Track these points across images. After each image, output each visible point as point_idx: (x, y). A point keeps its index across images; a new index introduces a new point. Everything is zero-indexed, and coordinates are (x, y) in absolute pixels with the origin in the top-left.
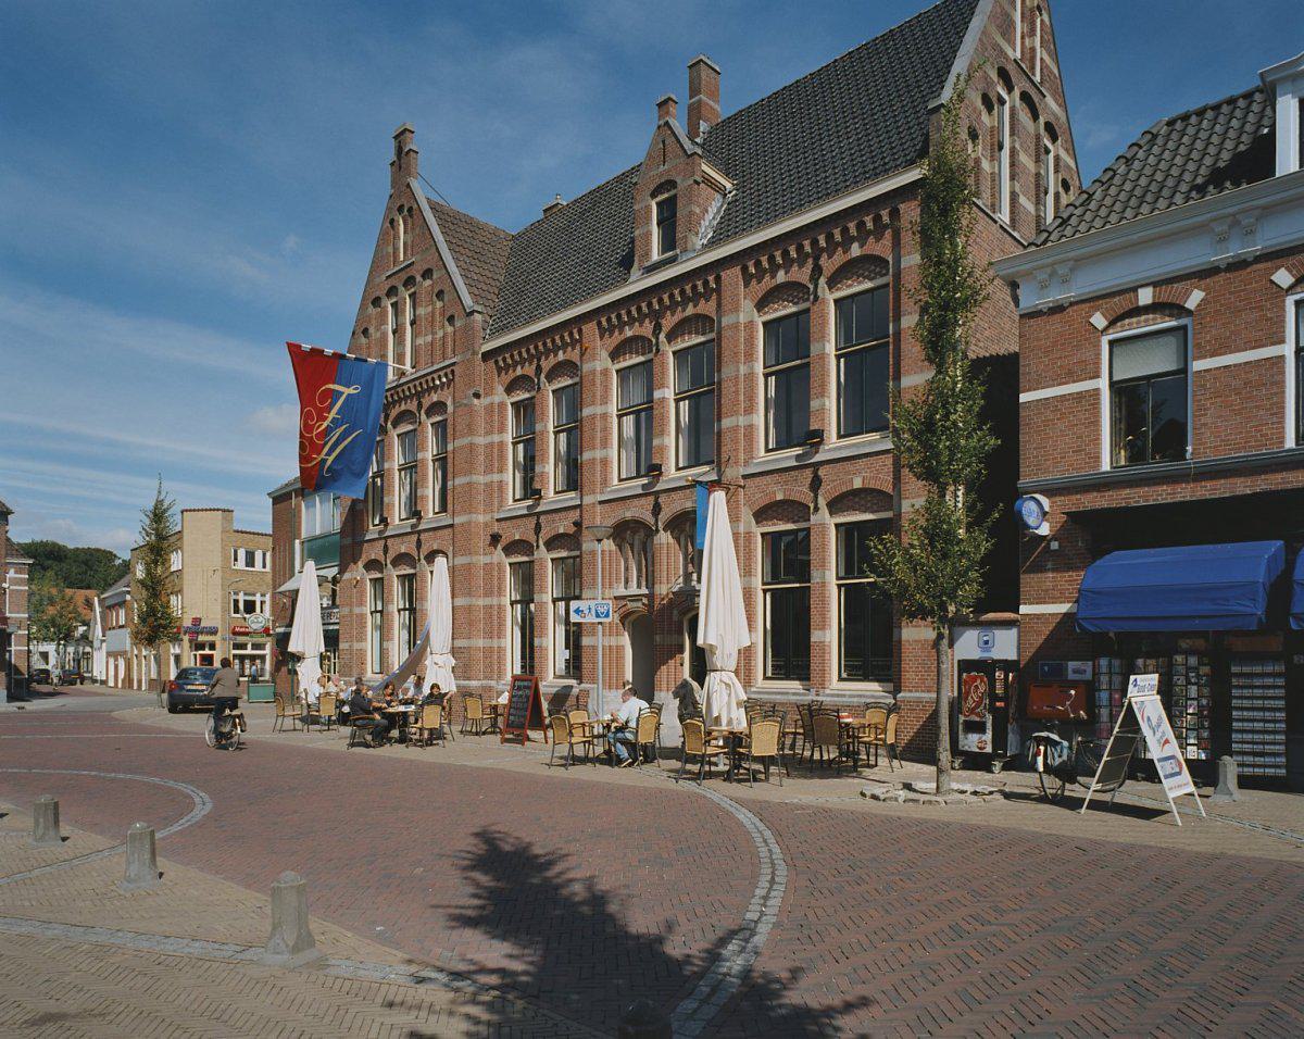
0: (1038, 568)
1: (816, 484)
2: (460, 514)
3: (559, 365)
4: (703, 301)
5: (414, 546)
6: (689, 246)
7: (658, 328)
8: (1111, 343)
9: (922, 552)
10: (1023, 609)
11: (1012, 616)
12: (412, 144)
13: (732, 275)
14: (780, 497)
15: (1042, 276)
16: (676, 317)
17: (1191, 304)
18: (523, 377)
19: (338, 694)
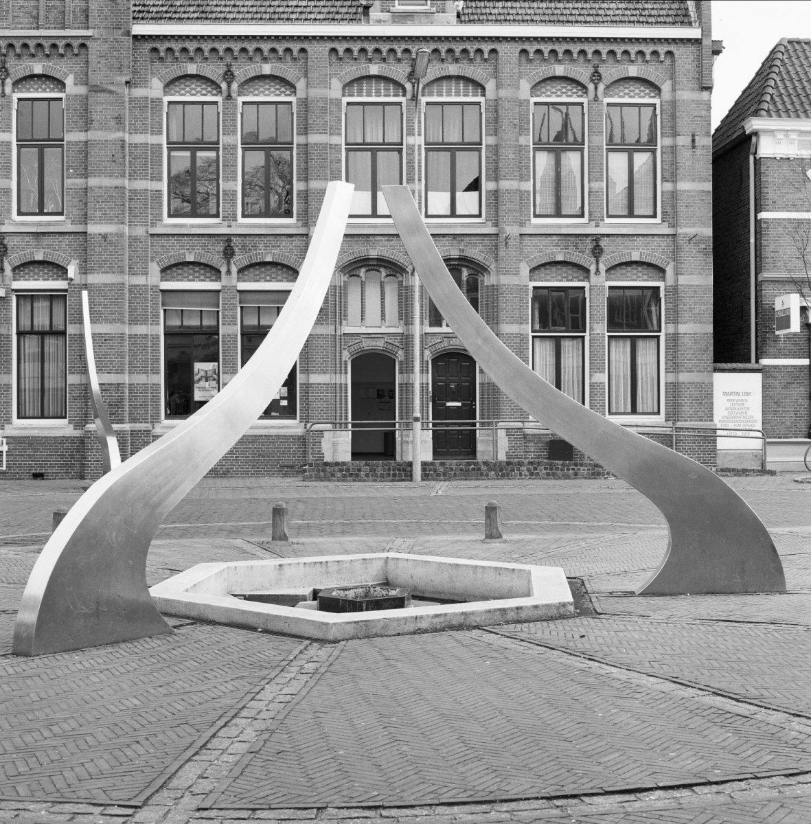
7: (596, 77)
13: (508, 53)
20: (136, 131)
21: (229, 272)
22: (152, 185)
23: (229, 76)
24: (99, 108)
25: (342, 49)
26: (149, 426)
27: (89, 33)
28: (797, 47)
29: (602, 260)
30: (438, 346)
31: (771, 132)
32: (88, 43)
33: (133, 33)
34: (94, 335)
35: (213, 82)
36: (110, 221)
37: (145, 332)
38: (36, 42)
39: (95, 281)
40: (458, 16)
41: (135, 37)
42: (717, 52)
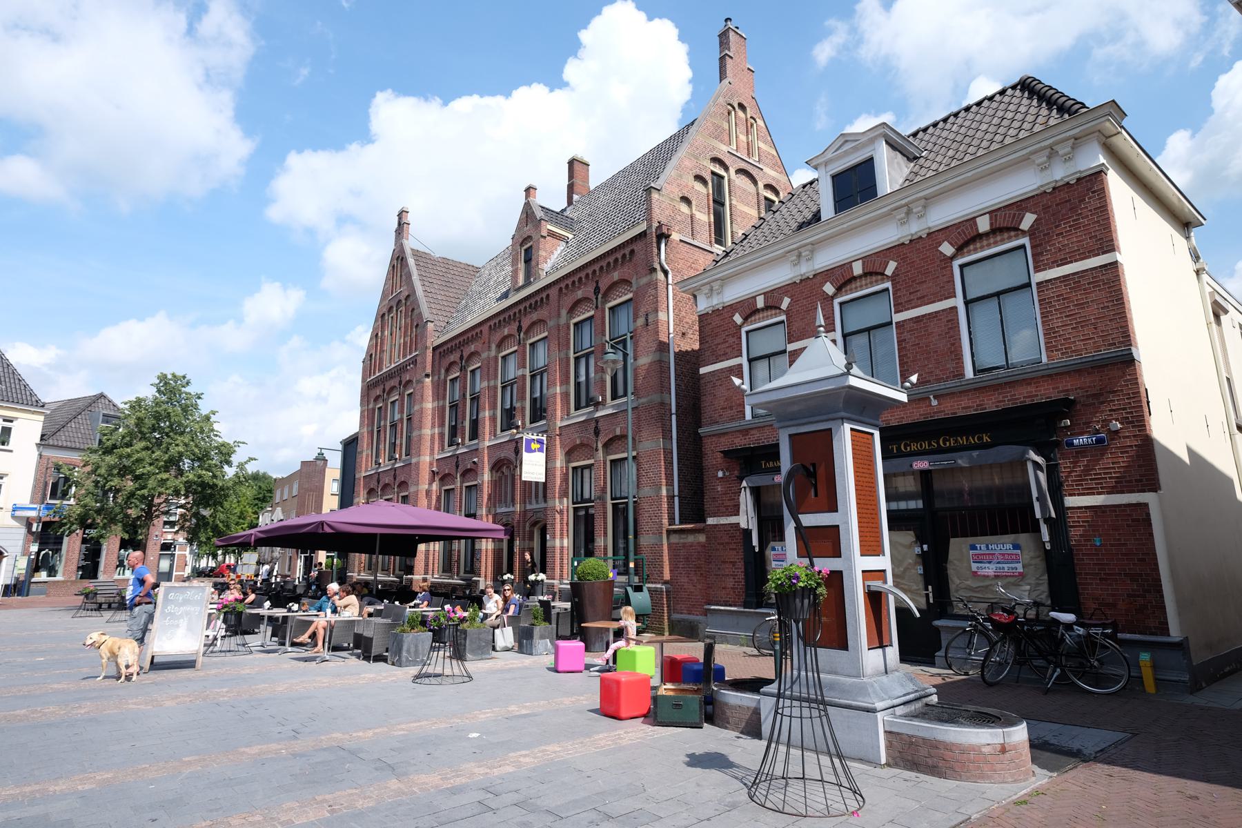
1: (597, 432)
3: (533, 324)
5: (392, 479)
8: (841, 304)
10: (711, 521)
12: (410, 218)
15: (901, 214)
18: (510, 336)
19: (1025, 613)
30: (532, 519)
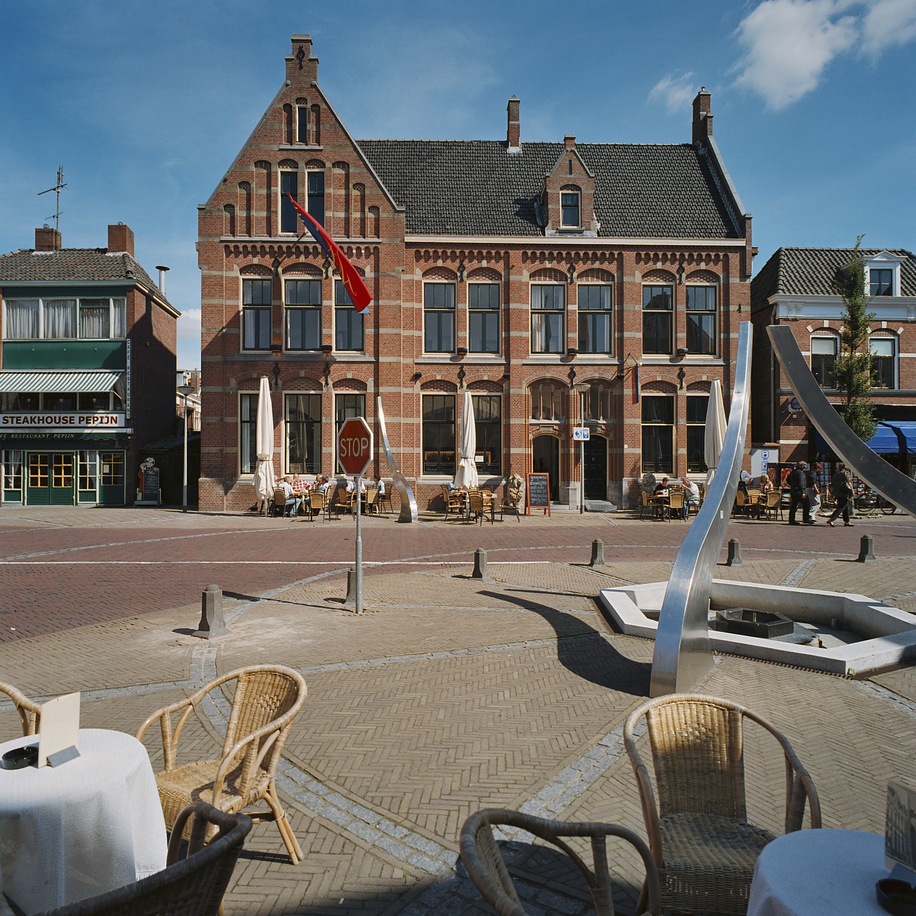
0: (787, 424)
2: (386, 354)
4: (493, 261)
6: (592, 227)
7: (681, 270)
9: (850, 413)
11: (776, 444)
13: (629, 256)
14: (659, 379)
16: (586, 266)
17: (899, 332)
20: (406, 300)
21: (462, 386)
22: (416, 333)
23: (462, 268)
24: (386, 286)
25: (531, 253)
26: (413, 479)
27: (380, 240)
28: (791, 252)
29: (684, 379)
31: (786, 302)
32: (379, 246)
33: (406, 241)
34: (386, 424)
35: (452, 271)
36: (393, 355)
37: (412, 422)
38: (260, 244)
39: (384, 391)
40: (598, 233)
41: (406, 243)
42: (754, 255)
